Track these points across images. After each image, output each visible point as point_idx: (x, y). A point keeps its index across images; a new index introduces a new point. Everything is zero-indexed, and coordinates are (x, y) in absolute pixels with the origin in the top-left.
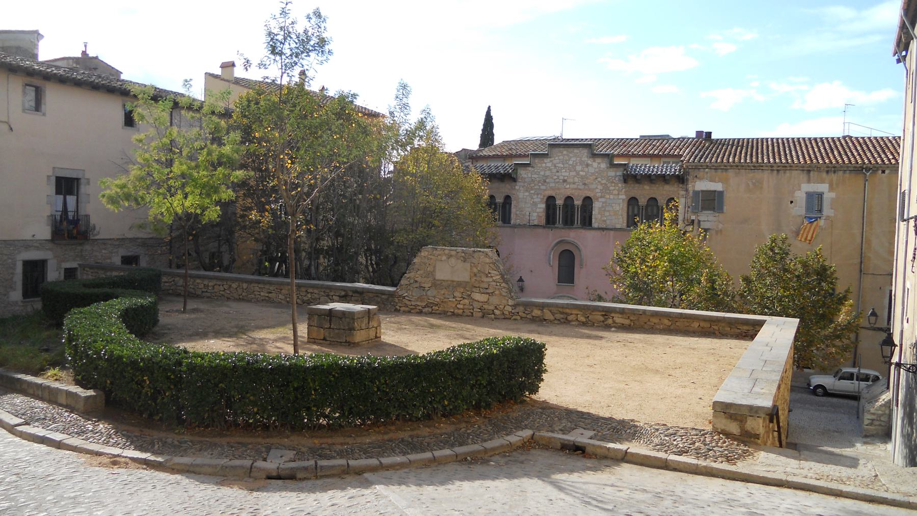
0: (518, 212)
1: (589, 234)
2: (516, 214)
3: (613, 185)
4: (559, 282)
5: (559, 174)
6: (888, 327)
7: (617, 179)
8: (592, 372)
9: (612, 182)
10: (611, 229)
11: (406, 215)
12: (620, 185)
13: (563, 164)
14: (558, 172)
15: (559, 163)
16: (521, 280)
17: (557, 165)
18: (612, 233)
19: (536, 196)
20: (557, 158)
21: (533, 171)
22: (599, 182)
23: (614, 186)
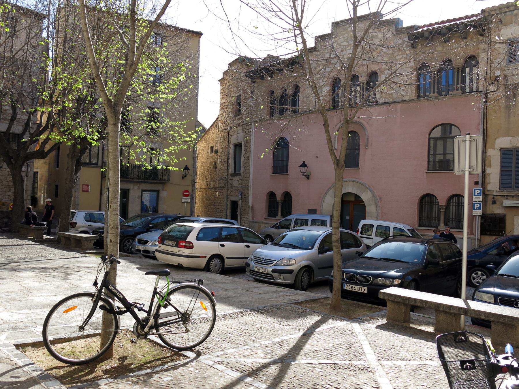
0: (305, 100)
1: (375, 110)
2: (303, 101)
3: (400, 53)
4: (428, 170)
5: (344, 53)
6: (126, 186)
7: (404, 46)
8: (226, 290)
9: (400, 50)
10: (398, 102)
11: (29, 94)
12: (408, 52)
13: (347, 42)
14: (342, 51)
15: (344, 41)
16: (304, 165)
17: (342, 44)
18: (399, 106)
19: (321, 81)
20: (342, 37)
21: (319, 55)
22: (385, 53)
23: (402, 54)
